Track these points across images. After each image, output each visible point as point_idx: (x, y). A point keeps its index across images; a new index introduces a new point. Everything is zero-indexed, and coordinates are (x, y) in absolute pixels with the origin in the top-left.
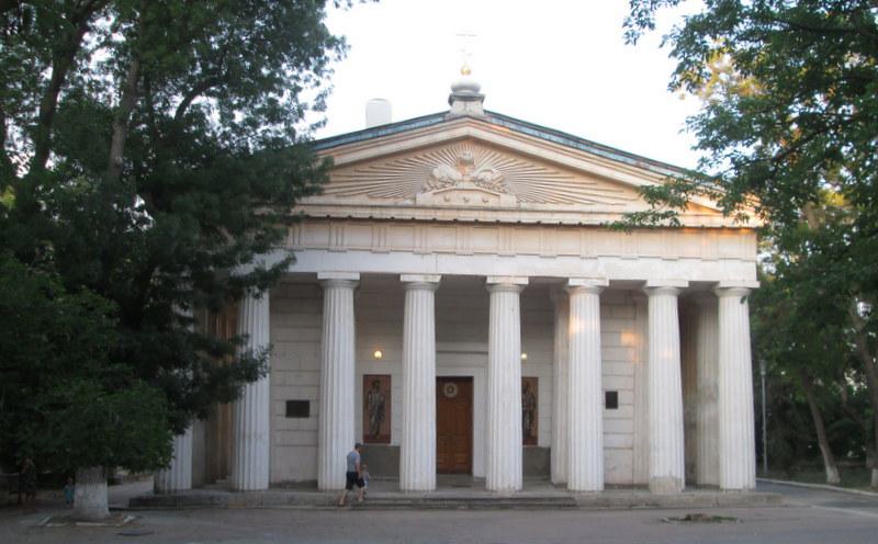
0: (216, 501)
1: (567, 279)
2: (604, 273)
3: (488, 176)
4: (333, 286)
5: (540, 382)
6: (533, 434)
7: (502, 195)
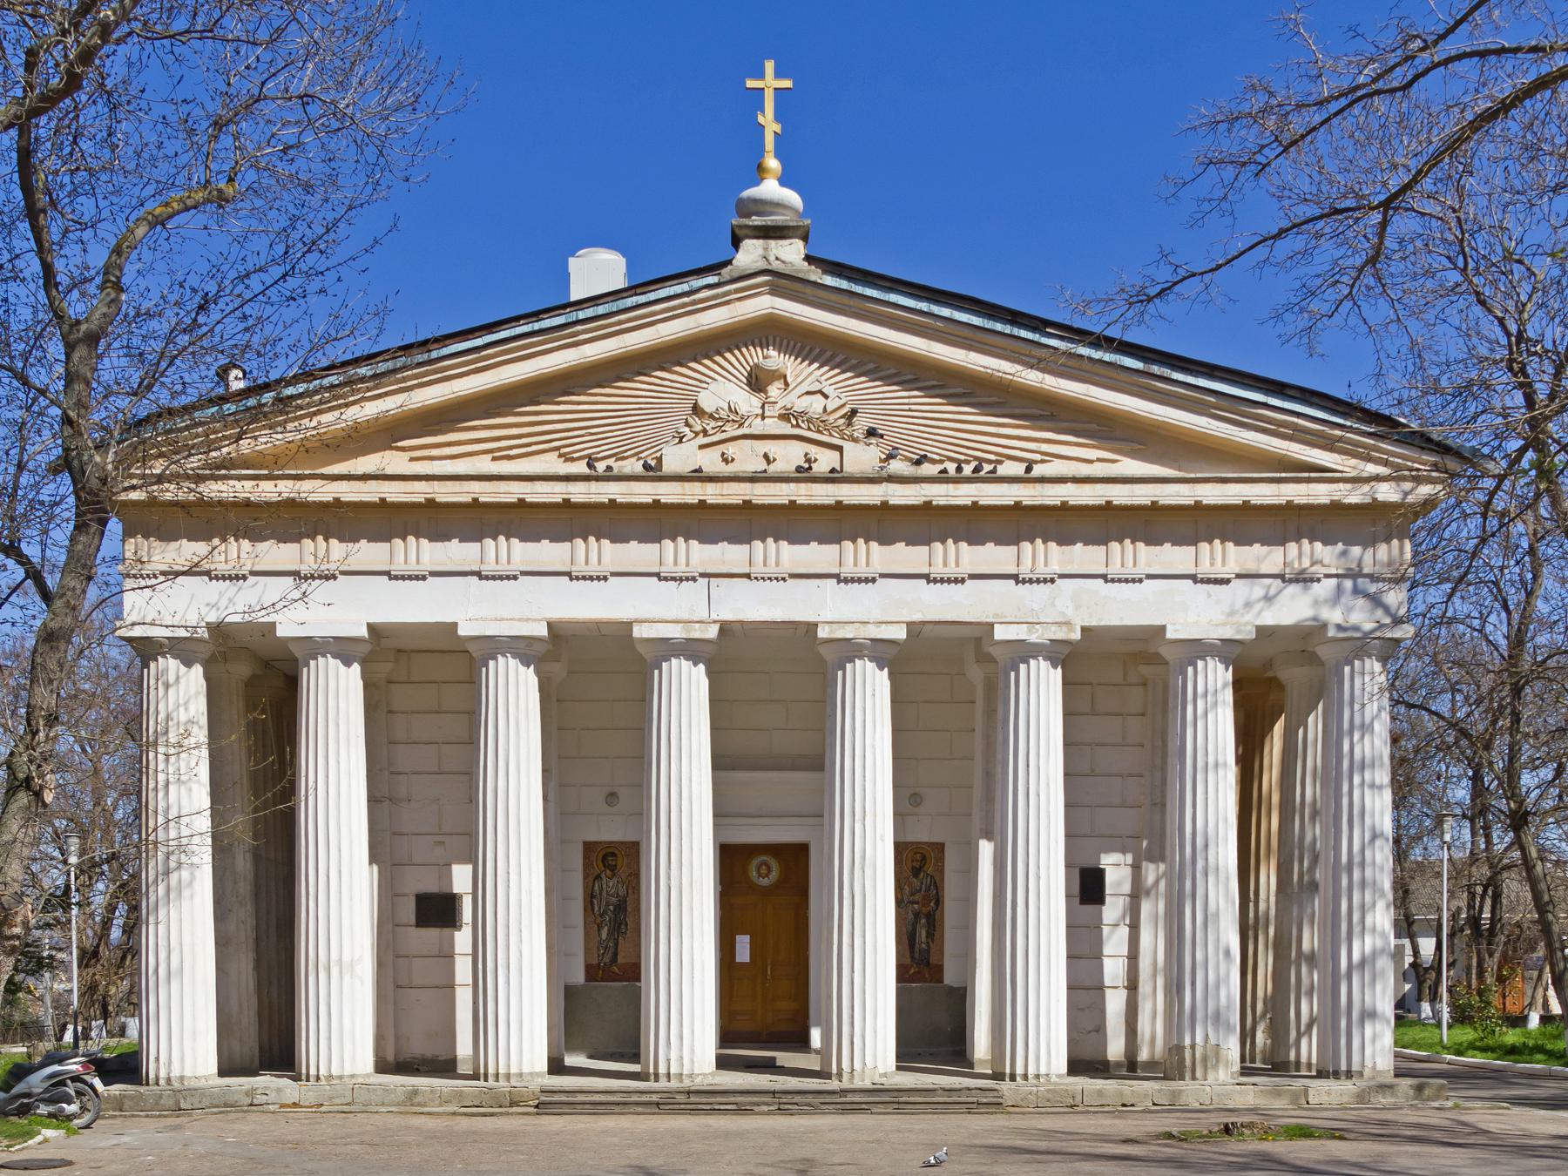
0: (259, 1099)
1: (990, 626)
2: (1070, 612)
3: (816, 405)
4: (1372, 609)
5: (592, 837)
6: (933, 960)
7: (848, 446)
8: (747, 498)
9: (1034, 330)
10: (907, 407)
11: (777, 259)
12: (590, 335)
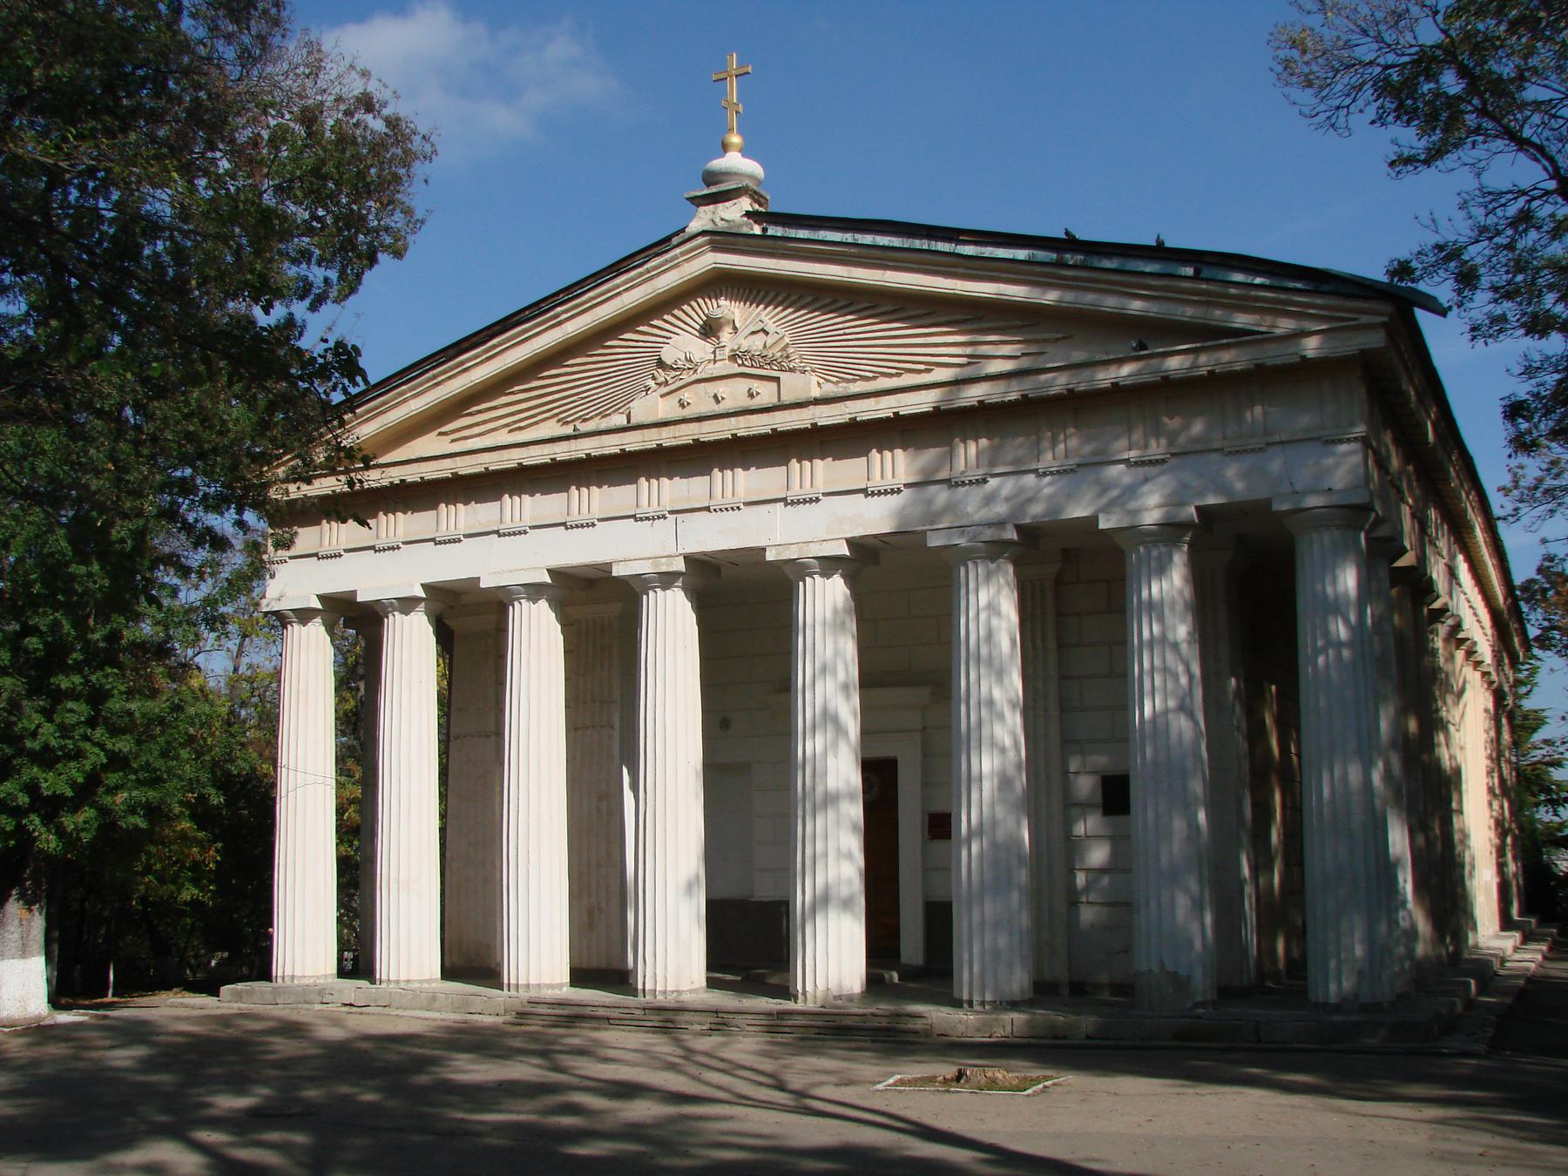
3: (757, 343)
7: (783, 376)
8: (696, 437)
9: (949, 240)
10: (842, 332)
11: (722, 219)
12: (569, 314)
